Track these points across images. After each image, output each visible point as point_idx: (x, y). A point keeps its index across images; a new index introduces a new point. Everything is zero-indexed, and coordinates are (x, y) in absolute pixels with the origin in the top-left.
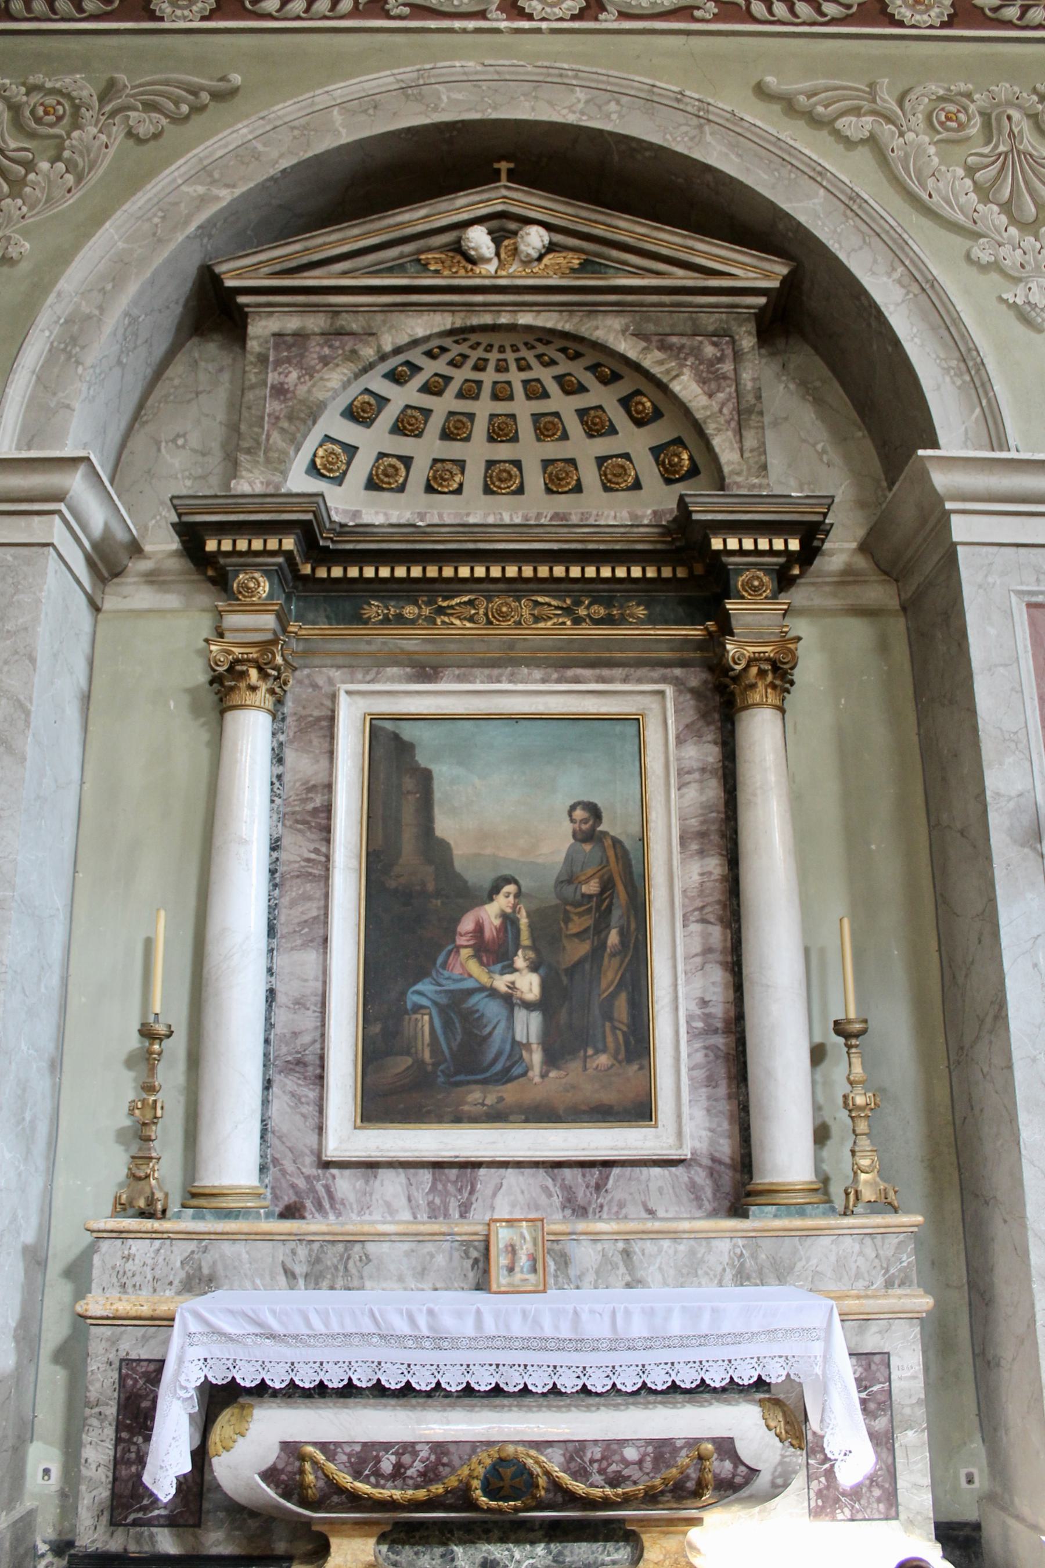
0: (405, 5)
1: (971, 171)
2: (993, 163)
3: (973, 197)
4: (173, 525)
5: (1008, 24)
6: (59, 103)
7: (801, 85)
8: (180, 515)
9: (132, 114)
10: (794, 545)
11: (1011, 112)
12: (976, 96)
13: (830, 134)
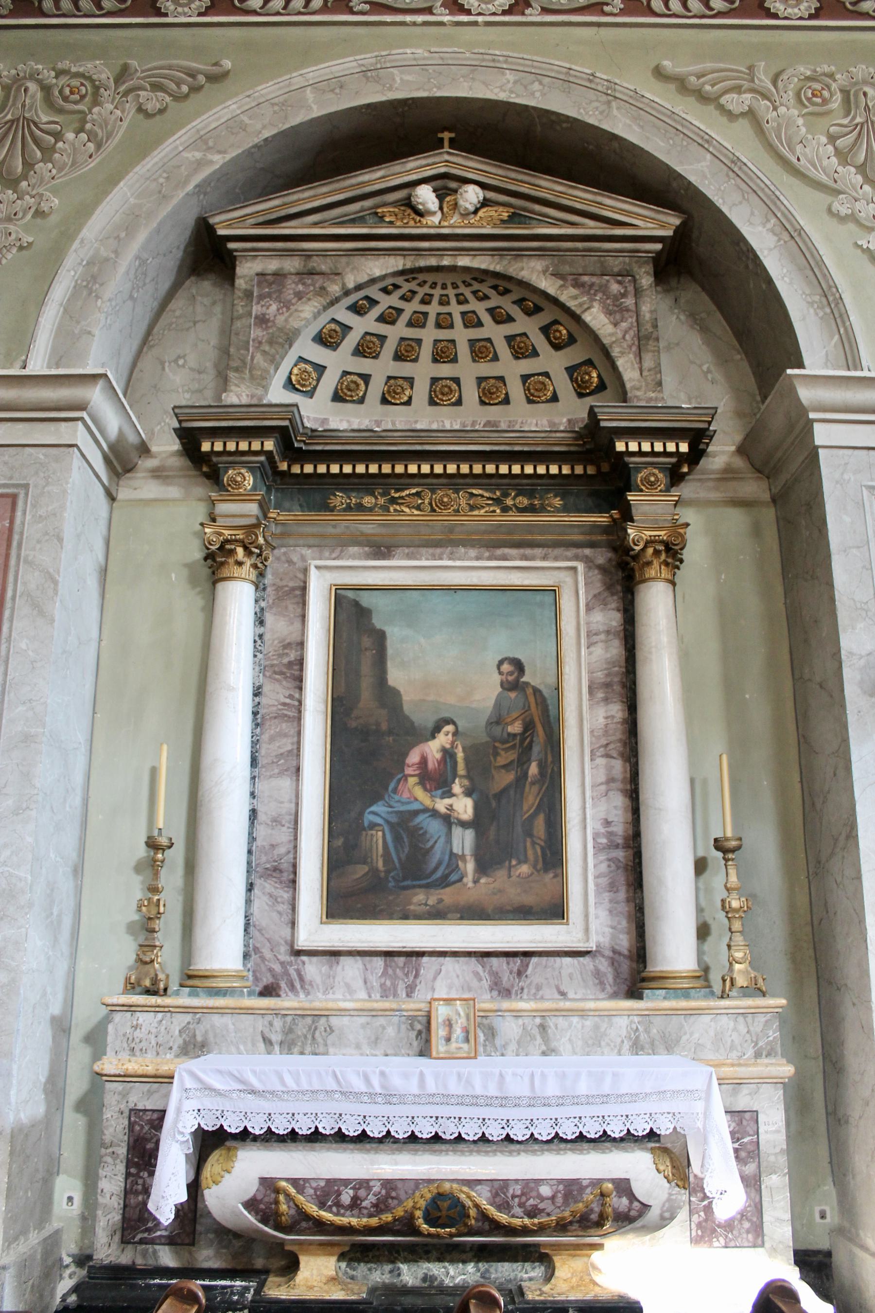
0: (365, 3)
1: (832, 139)
2: (855, 129)
3: (834, 160)
4: (175, 430)
6: (82, 84)
8: (180, 422)
9: (142, 93)
10: (684, 447)
11: (867, 89)
13: (716, 108)
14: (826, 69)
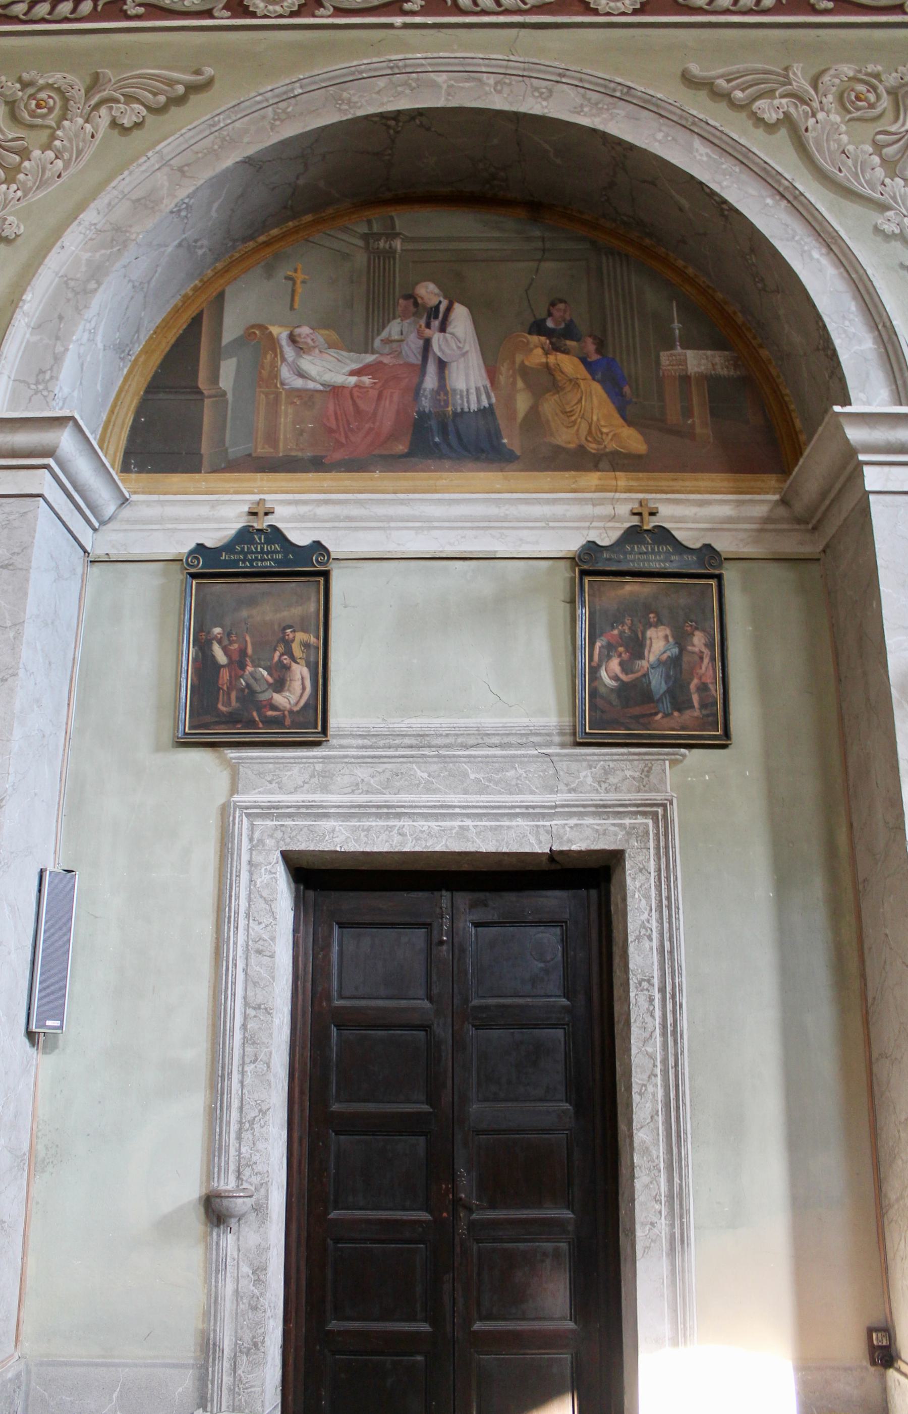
0: (140, 5)
1: (878, 147)
5: (16, 20)
6: (50, 97)
7: (175, 74)
12: (883, 77)
13: (749, 117)
14: (870, 68)
